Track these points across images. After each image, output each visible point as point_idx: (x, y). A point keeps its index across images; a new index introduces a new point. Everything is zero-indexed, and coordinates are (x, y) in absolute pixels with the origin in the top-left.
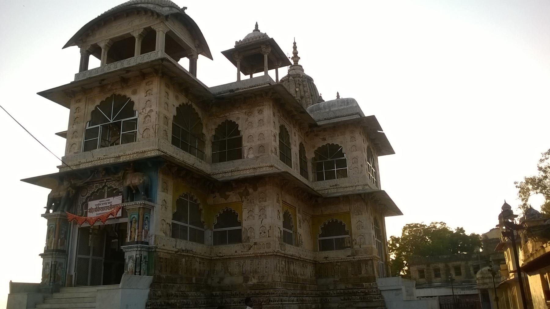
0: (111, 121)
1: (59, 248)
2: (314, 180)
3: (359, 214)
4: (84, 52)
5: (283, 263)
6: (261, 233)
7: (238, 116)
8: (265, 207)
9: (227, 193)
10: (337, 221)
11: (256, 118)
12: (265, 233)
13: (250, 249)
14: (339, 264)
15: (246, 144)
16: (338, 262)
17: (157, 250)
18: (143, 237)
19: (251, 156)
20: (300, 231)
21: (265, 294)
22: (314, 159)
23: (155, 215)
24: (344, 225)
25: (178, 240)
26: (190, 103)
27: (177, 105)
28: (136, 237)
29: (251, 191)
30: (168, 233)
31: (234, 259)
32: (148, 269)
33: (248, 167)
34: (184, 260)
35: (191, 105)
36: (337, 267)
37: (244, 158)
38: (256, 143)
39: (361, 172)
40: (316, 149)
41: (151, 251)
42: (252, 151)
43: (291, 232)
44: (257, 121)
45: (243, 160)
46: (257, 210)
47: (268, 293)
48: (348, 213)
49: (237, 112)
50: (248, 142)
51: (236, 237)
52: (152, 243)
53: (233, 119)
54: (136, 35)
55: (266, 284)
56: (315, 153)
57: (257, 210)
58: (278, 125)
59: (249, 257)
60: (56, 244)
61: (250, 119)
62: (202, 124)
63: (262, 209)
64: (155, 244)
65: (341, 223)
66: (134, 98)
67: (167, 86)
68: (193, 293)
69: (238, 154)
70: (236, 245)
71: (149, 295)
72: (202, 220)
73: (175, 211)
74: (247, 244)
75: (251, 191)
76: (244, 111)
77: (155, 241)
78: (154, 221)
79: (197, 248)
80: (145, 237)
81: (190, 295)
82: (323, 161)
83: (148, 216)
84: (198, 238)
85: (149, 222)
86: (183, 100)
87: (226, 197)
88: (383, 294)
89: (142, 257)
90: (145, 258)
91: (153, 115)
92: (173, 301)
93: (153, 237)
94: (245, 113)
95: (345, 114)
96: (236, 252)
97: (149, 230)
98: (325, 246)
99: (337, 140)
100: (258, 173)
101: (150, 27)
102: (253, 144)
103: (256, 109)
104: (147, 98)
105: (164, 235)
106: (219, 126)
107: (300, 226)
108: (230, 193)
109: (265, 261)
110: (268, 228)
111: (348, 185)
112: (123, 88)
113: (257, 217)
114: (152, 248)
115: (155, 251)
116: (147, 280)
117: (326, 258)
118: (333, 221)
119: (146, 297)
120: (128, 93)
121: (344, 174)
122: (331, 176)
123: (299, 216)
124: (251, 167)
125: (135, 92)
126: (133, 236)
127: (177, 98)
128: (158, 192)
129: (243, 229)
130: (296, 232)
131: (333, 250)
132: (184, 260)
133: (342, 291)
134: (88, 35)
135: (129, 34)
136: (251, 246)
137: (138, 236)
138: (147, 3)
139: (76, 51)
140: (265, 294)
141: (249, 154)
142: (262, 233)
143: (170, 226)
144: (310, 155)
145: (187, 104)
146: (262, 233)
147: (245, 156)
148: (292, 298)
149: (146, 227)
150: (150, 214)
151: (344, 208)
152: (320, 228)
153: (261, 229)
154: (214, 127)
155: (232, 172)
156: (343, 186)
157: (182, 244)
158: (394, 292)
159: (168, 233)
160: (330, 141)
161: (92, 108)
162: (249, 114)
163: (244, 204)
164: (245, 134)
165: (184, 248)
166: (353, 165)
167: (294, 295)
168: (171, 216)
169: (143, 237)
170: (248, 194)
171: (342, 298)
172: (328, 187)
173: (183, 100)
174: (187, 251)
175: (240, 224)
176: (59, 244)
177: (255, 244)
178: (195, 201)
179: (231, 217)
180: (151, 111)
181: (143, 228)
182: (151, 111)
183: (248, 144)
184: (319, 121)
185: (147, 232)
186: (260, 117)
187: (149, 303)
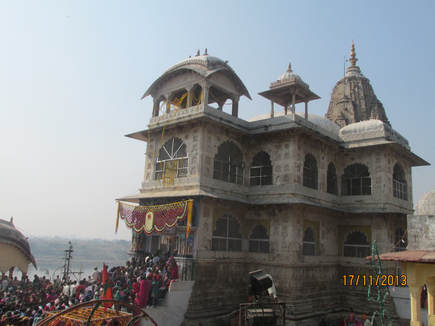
0: (172, 159)
1: (139, 250)
2: (343, 194)
3: (379, 229)
4: (156, 101)
5: (301, 271)
6: (283, 247)
7: (270, 148)
8: (286, 227)
9: (260, 212)
10: (360, 232)
11: (283, 151)
12: (286, 247)
13: (274, 259)
14: (359, 269)
15: (275, 173)
16: (358, 267)
17: (198, 261)
18: (188, 252)
19: (278, 183)
20: (322, 241)
21: (283, 296)
22: (343, 176)
23: (197, 235)
24: (366, 237)
25: (217, 252)
26: (231, 140)
27: (218, 144)
28: (183, 252)
29: (277, 212)
30: (209, 247)
31: (264, 265)
32: (192, 275)
33: (276, 192)
34: (222, 266)
35: (232, 142)
36: (357, 271)
37: (273, 185)
38: (283, 173)
39: (383, 192)
40: (346, 167)
41: (194, 263)
42: (279, 179)
43: (314, 243)
44: (284, 154)
45: (272, 186)
46: (280, 228)
47: (285, 296)
48: (370, 227)
49: (269, 145)
50: (277, 171)
51: (265, 248)
52: (195, 258)
53: (267, 151)
54: (188, 90)
55: (284, 288)
56: (345, 170)
57: (280, 228)
58: (303, 156)
59: (273, 266)
60: (137, 247)
61: (279, 152)
62: (242, 155)
63: (285, 228)
64: (197, 258)
65: (363, 234)
66: (186, 142)
67: (210, 132)
68: (229, 290)
69: (268, 181)
70: (264, 254)
71: (192, 294)
72: (240, 232)
73: (215, 229)
74: (272, 255)
75: (277, 212)
76: (275, 144)
77: (197, 255)
78: (197, 239)
79: (234, 255)
80: (190, 252)
81: (226, 291)
82: (351, 178)
83: (192, 236)
84: (235, 247)
85: (193, 240)
86: (224, 139)
87: (259, 215)
88: (395, 301)
89: (188, 267)
90: (189, 267)
91: (198, 157)
92: (210, 298)
93: (196, 252)
94: (276, 146)
95: (371, 137)
96: (264, 260)
97: (193, 246)
98: (349, 252)
99: (364, 161)
100: (281, 201)
101: (198, 84)
102: (280, 174)
103: (284, 143)
104: (195, 143)
105: (205, 249)
106: (256, 155)
107: (323, 237)
108: (262, 212)
109: (284, 270)
110: (288, 245)
111: (370, 202)
112: (179, 133)
113: (280, 235)
114: (195, 260)
115: (197, 262)
116: (191, 283)
117: (348, 262)
118: (356, 231)
119: (190, 296)
120: (182, 137)
121: (368, 192)
122: (356, 192)
123: (322, 229)
124: (278, 193)
125: (187, 137)
126: (182, 251)
127: (218, 139)
128: (200, 218)
129: (270, 242)
130: (318, 243)
131: (355, 256)
132: (222, 266)
133: (359, 292)
134: (158, 89)
135: (184, 88)
136: (275, 257)
137: (185, 251)
138: (196, 64)
139: (150, 99)
140: (283, 296)
141: (277, 182)
142: (284, 248)
143: (210, 242)
144: (340, 173)
145: (228, 142)
146: (284, 248)
147: (274, 182)
148: (307, 300)
149: (191, 245)
150: (194, 234)
151: (367, 222)
152: (345, 236)
153: (283, 244)
154: (252, 156)
155: (263, 195)
156: (367, 202)
157: (219, 254)
158: (404, 300)
159: (209, 247)
160: (358, 161)
161: (159, 147)
162: (278, 147)
163: (272, 222)
164: (275, 164)
165: (222, 257)
166: (377, 184)
167: (309, 297)
168: (211, 233)
169: (188, 252)
170: (274, 214)
171: (359, 298)
172: (354, 202)
173: (224, 139)
174: (224, 258)
175: (268, 237)
176: (139, 247)
177: (278, 255)
178: (234, 218)
179: (262, 232)
180: (197, 154)
181: (188, 245)
182: (197, 154)
183: (276, 173)
184: (350, 142)
185: (191, 248)
186: (287, 151)
187: (191, 300)
